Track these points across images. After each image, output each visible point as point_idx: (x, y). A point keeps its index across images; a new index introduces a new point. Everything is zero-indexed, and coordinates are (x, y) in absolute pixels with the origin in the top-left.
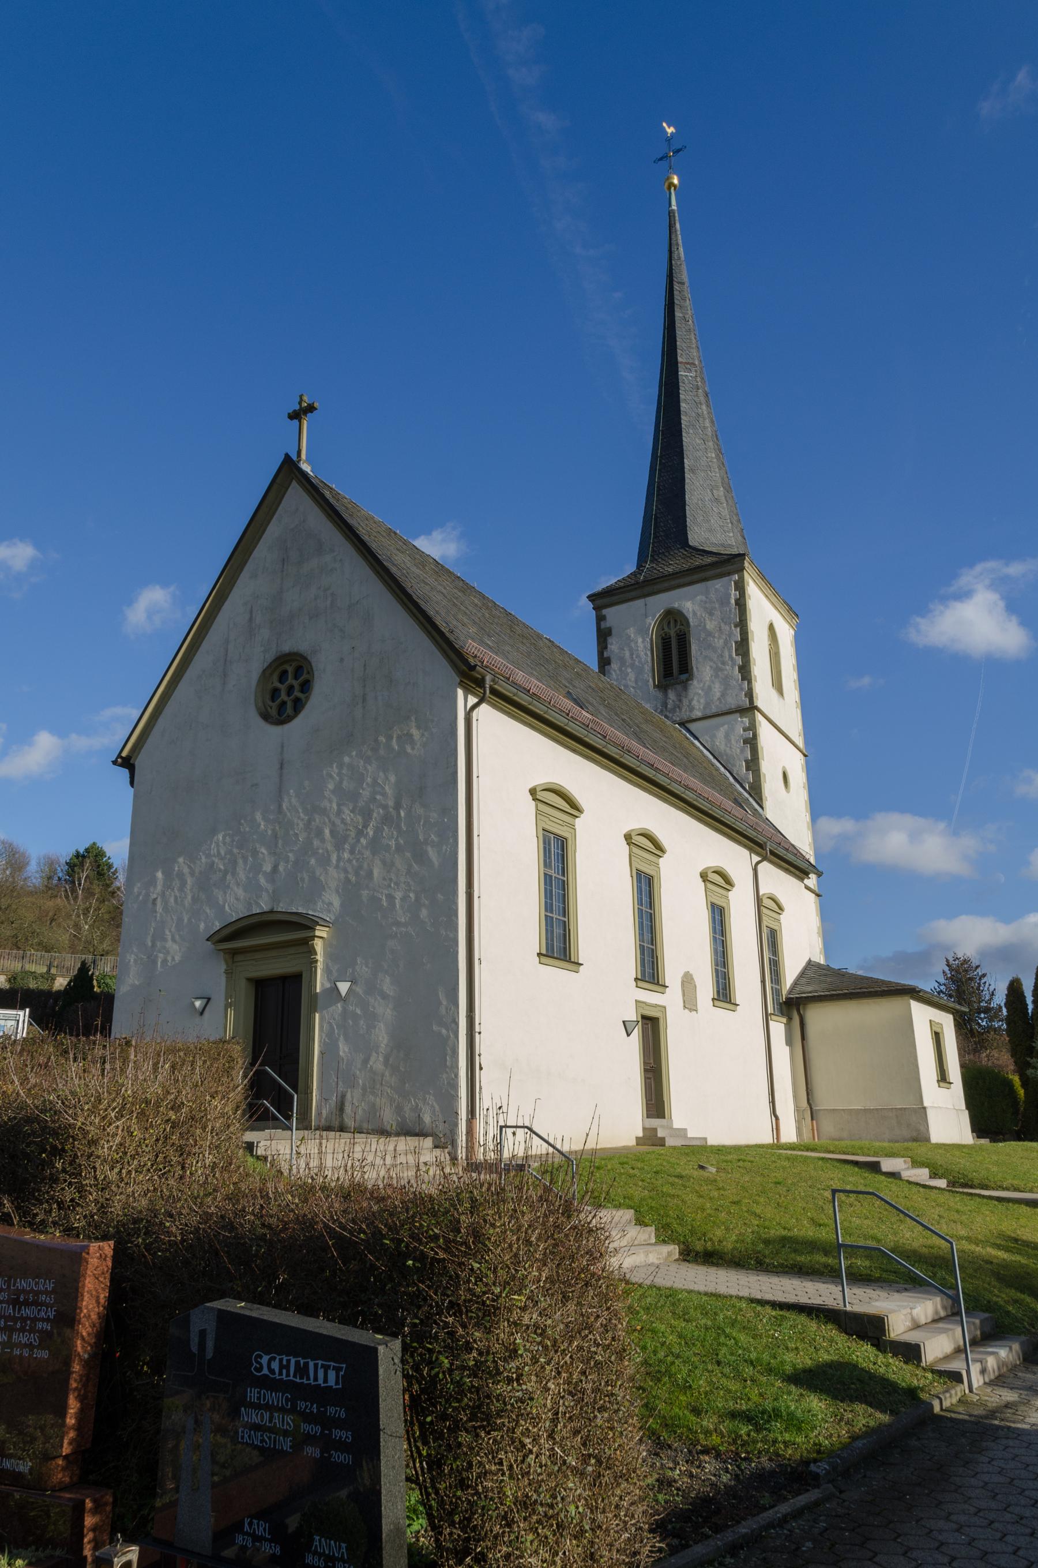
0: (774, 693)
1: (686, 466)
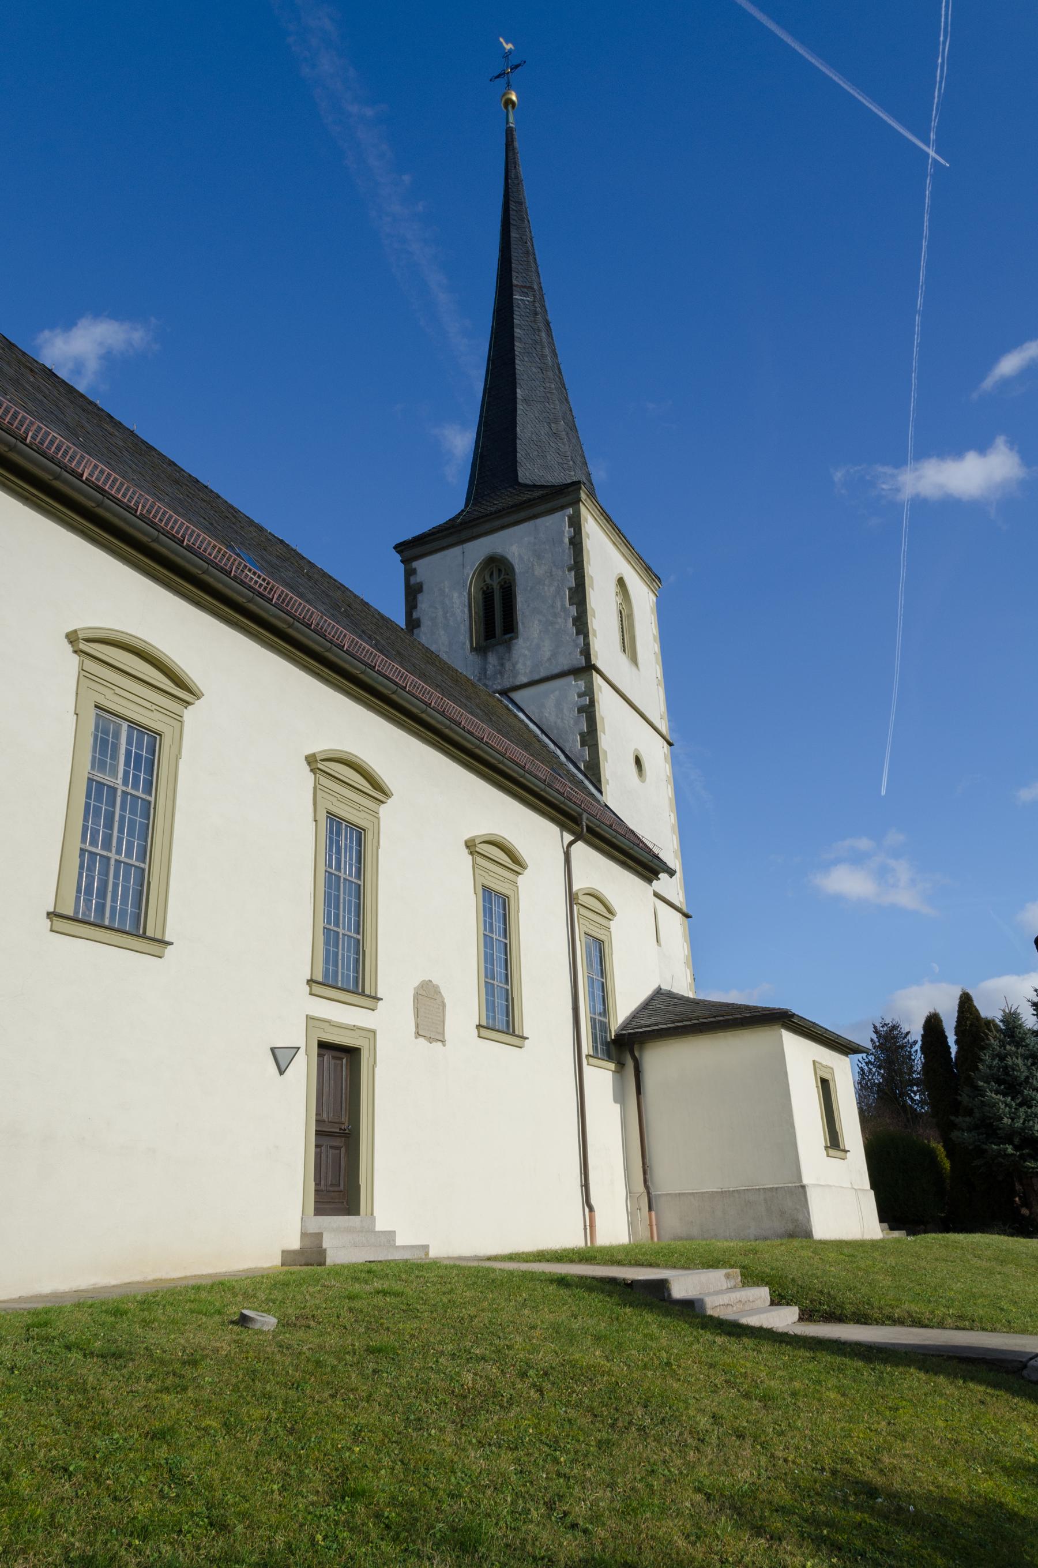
0: (623, 659)
1: (518, 396)
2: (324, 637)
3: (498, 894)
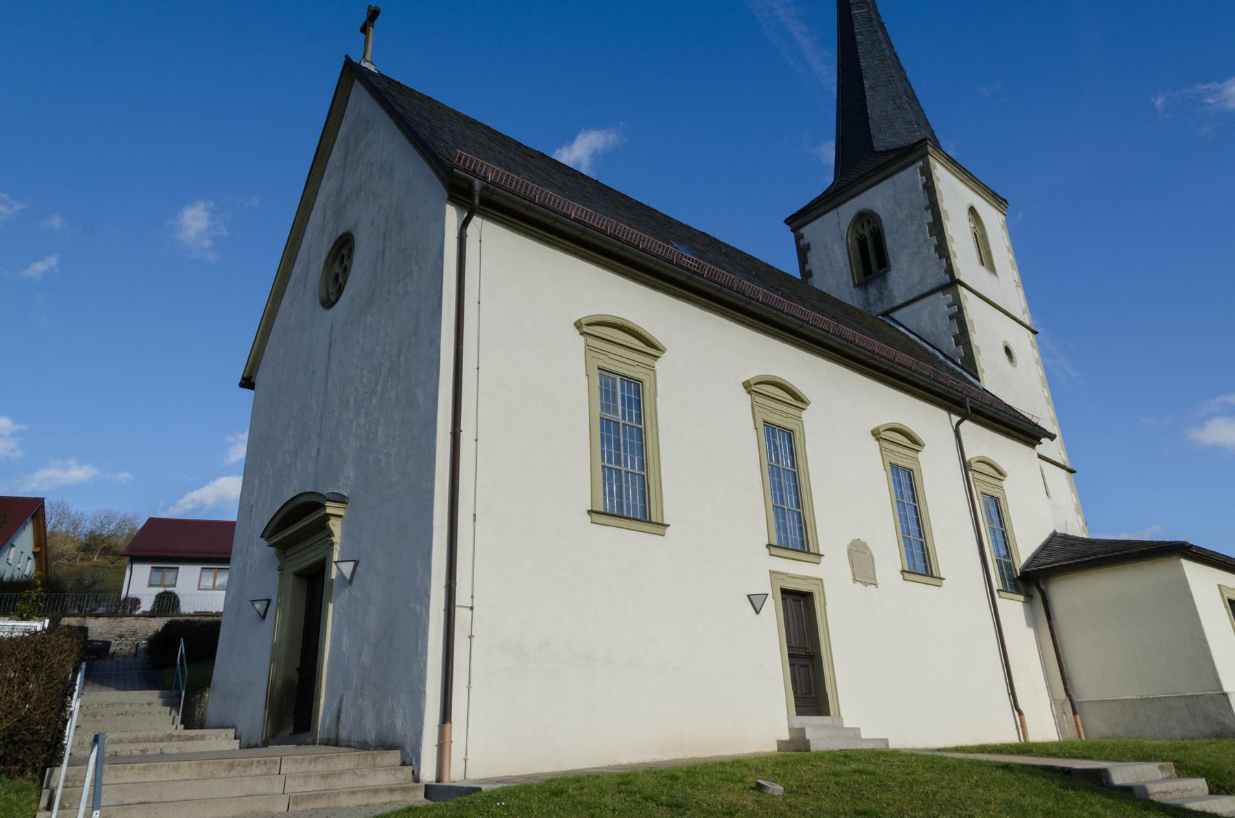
0: (983, 272)
2: (743, 294)
3: (903, 468)
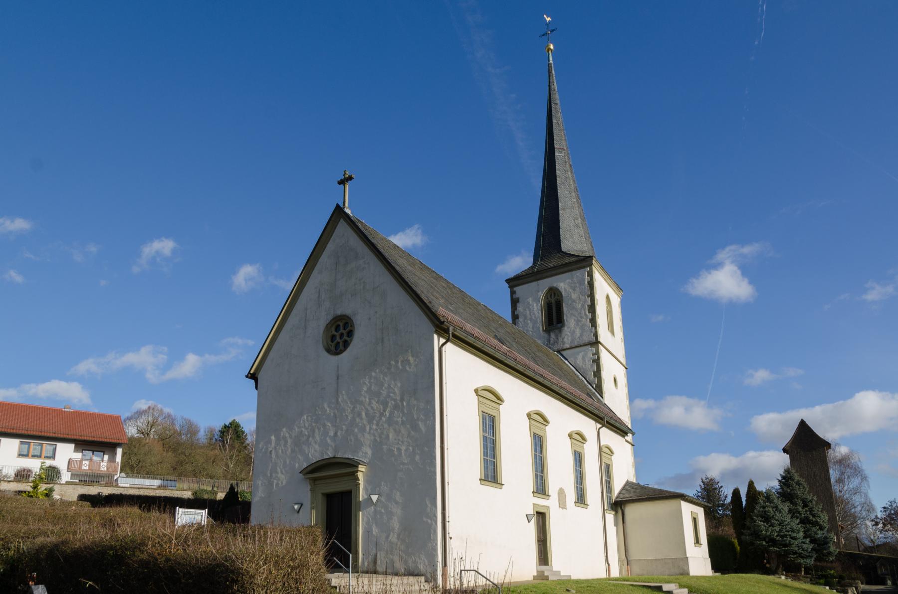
0: (609, 334)
